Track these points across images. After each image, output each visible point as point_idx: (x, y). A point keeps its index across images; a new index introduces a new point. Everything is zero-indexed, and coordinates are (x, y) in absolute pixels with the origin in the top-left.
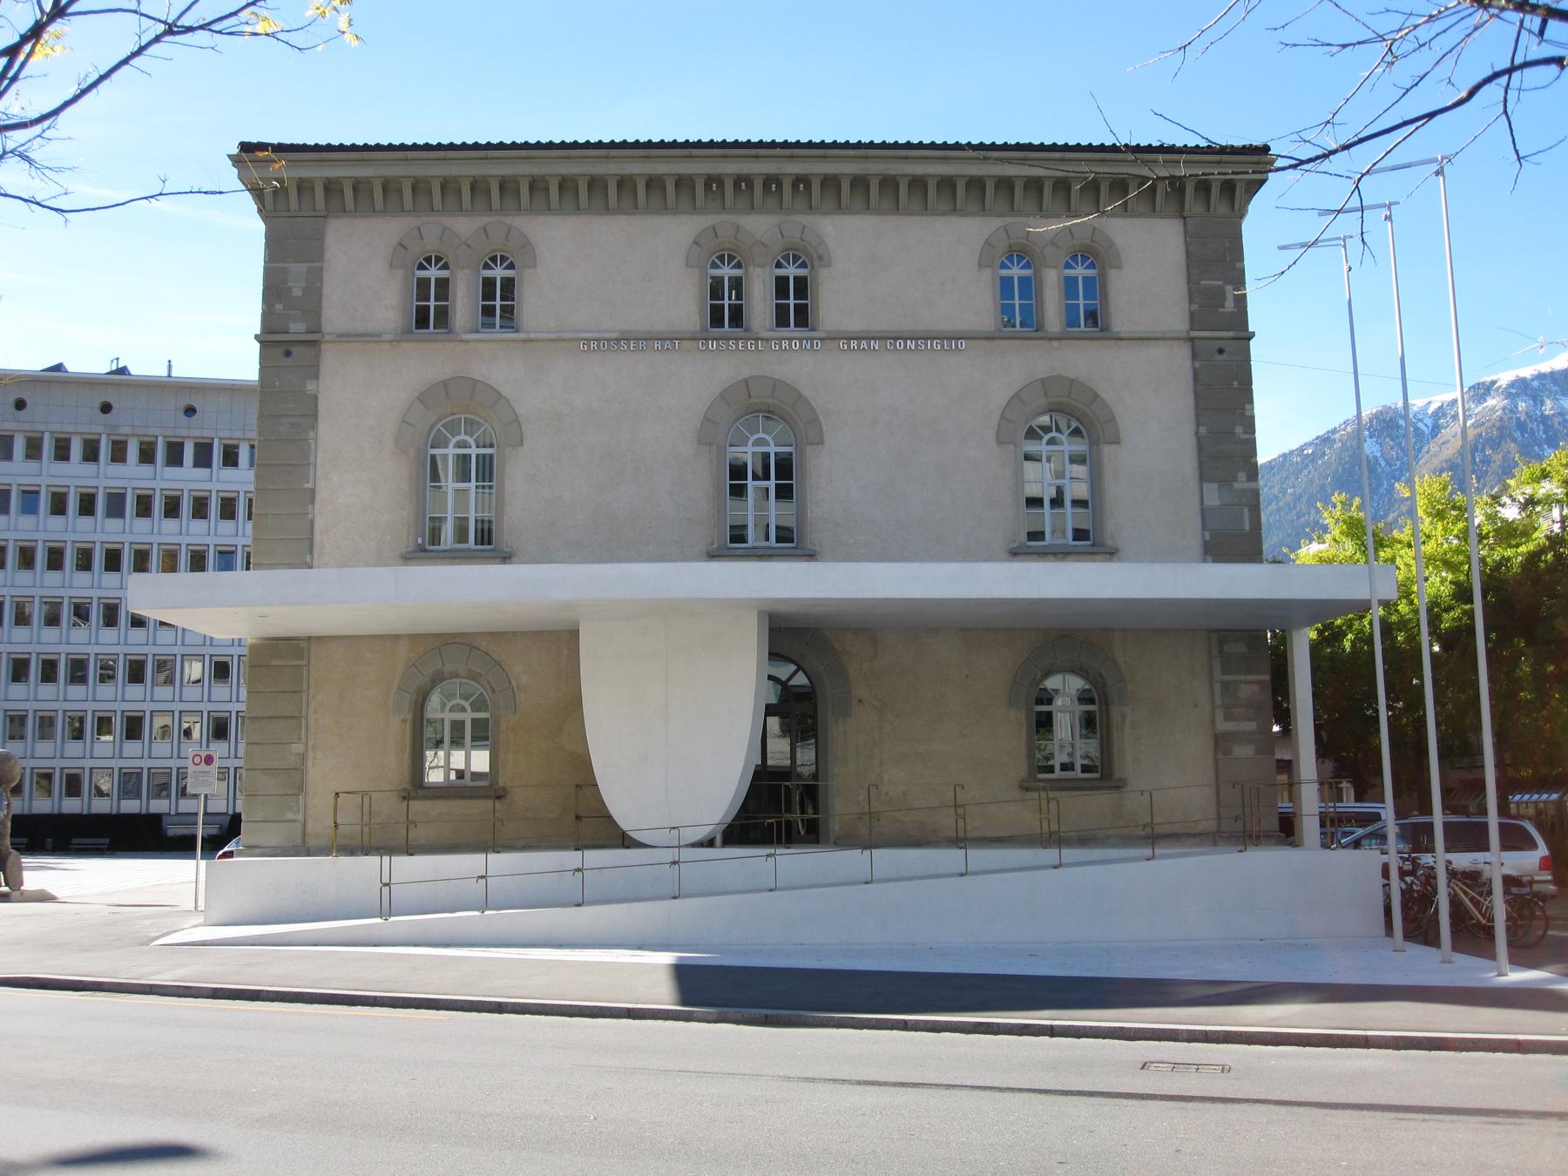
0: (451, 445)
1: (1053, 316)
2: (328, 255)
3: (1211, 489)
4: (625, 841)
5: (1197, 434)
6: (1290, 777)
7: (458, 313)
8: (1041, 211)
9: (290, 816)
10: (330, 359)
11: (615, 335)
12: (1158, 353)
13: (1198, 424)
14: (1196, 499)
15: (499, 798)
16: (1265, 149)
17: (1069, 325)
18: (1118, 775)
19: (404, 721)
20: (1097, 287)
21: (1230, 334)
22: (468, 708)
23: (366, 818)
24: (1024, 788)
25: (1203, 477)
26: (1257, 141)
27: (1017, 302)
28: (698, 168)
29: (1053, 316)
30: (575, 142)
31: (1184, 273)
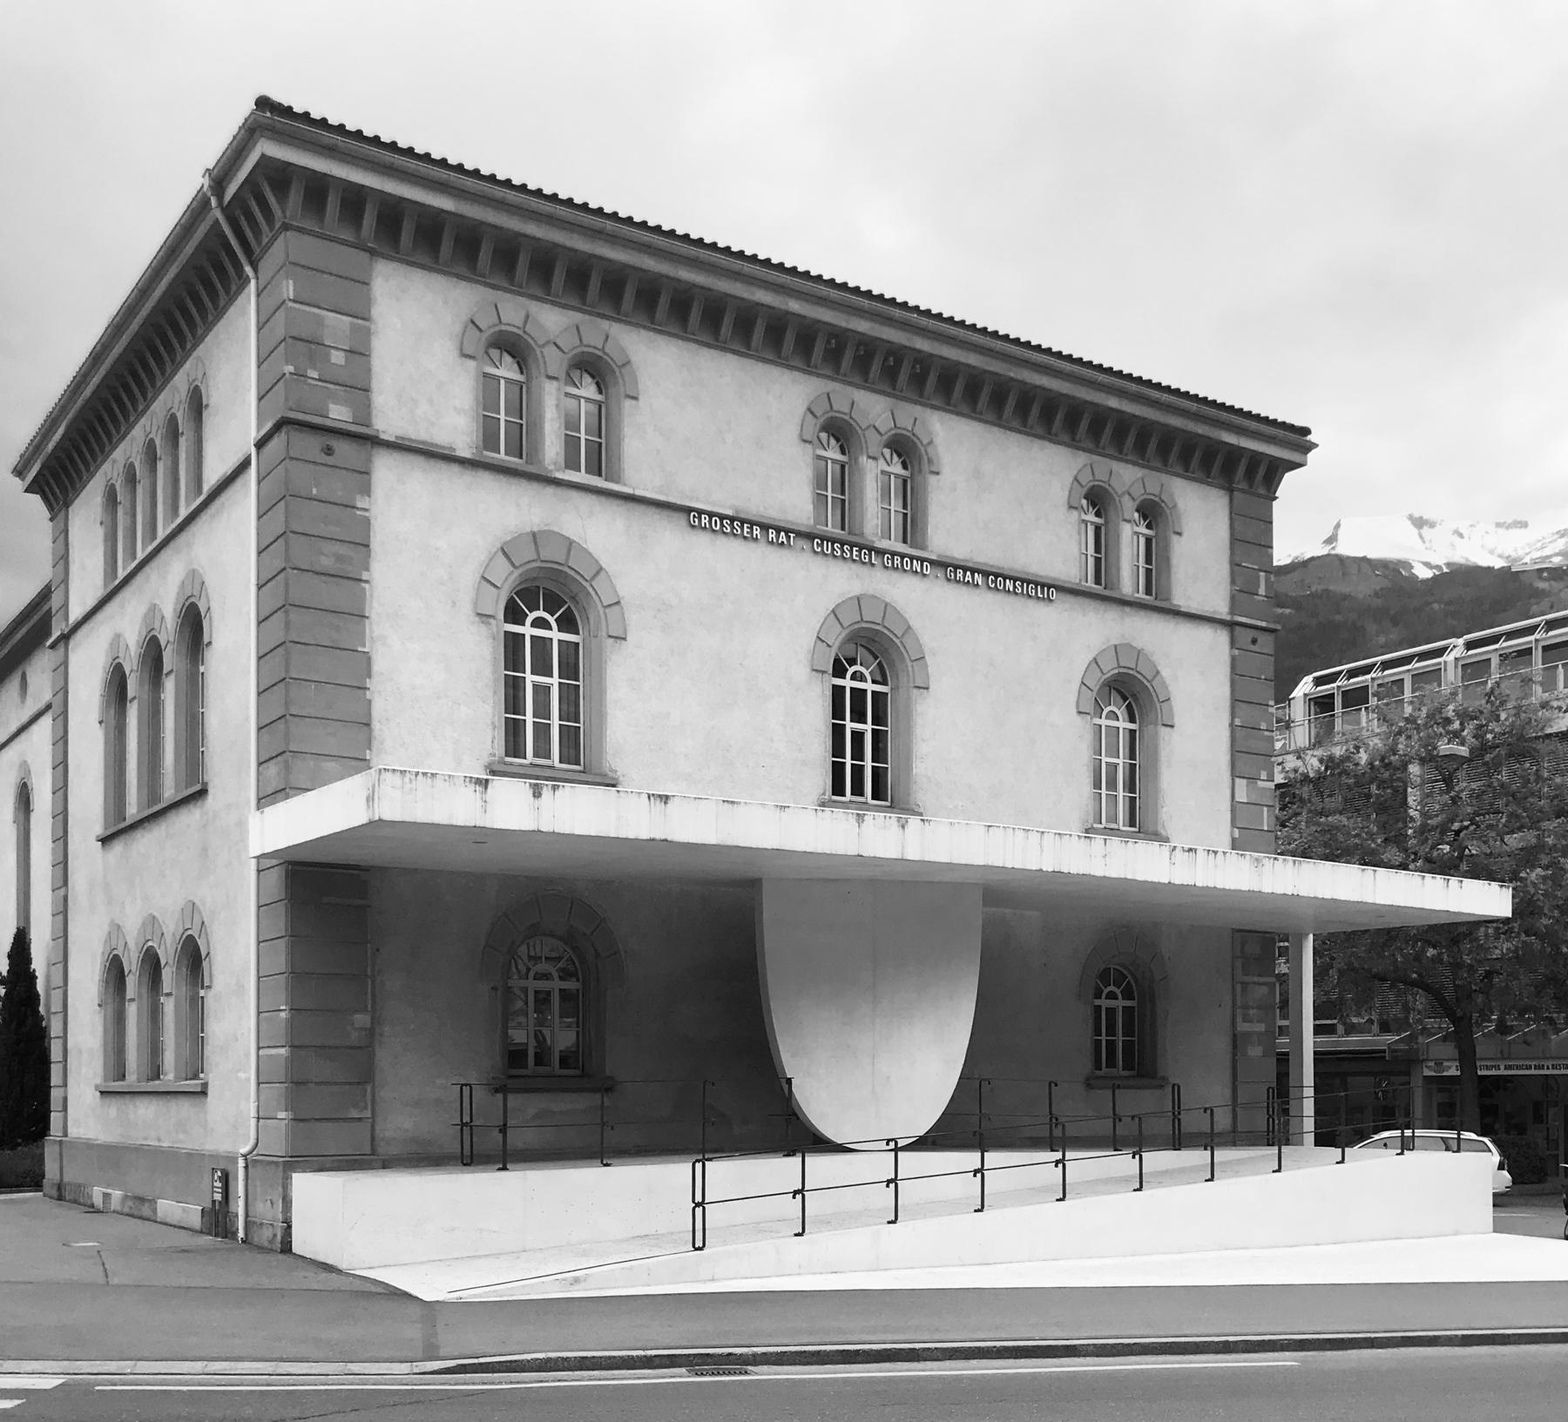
0: (529, 621)
1: (552, 449)
2: (375, 312)
3: (1241, 784)
4: (822, 1145)
5: (1231, 725)
6: (505, 1035)
7: (548, 442)
8: (546, 295)
9: (354, 1114)
10: (385, 469)
11: (730, 512)
12: (1206, 634)
13: (1233, 715)
14: (1228, 792)
15: (608, 1090)
16: (1305, 431)
17: (486, 448)
18: (1161, 1074)
19: (494, 989)
20: (604, 422)
21: (1264, 624)
22: (556, 975)
23: (466, 1119)
24: (1089, 1084)
25: (1234, 775)
26: (1298, 422)
27: (502, 417)
28: (1194, 406)
29: (552, 449)
30: (342, 126)
31: (1228, 552)
